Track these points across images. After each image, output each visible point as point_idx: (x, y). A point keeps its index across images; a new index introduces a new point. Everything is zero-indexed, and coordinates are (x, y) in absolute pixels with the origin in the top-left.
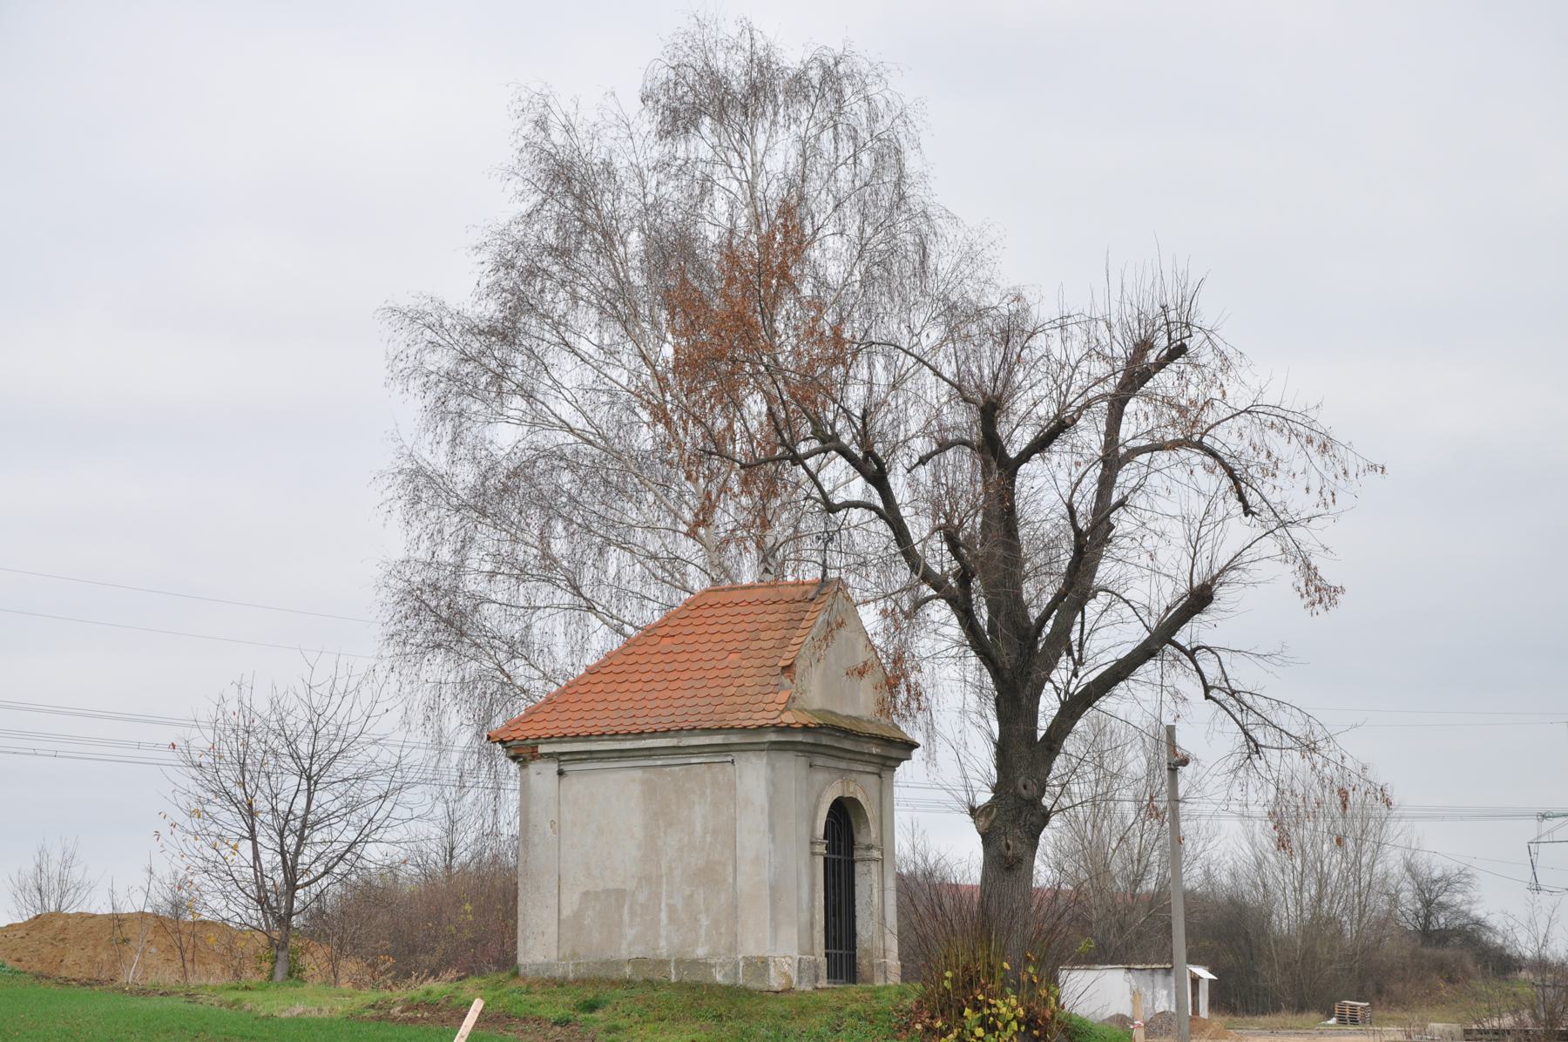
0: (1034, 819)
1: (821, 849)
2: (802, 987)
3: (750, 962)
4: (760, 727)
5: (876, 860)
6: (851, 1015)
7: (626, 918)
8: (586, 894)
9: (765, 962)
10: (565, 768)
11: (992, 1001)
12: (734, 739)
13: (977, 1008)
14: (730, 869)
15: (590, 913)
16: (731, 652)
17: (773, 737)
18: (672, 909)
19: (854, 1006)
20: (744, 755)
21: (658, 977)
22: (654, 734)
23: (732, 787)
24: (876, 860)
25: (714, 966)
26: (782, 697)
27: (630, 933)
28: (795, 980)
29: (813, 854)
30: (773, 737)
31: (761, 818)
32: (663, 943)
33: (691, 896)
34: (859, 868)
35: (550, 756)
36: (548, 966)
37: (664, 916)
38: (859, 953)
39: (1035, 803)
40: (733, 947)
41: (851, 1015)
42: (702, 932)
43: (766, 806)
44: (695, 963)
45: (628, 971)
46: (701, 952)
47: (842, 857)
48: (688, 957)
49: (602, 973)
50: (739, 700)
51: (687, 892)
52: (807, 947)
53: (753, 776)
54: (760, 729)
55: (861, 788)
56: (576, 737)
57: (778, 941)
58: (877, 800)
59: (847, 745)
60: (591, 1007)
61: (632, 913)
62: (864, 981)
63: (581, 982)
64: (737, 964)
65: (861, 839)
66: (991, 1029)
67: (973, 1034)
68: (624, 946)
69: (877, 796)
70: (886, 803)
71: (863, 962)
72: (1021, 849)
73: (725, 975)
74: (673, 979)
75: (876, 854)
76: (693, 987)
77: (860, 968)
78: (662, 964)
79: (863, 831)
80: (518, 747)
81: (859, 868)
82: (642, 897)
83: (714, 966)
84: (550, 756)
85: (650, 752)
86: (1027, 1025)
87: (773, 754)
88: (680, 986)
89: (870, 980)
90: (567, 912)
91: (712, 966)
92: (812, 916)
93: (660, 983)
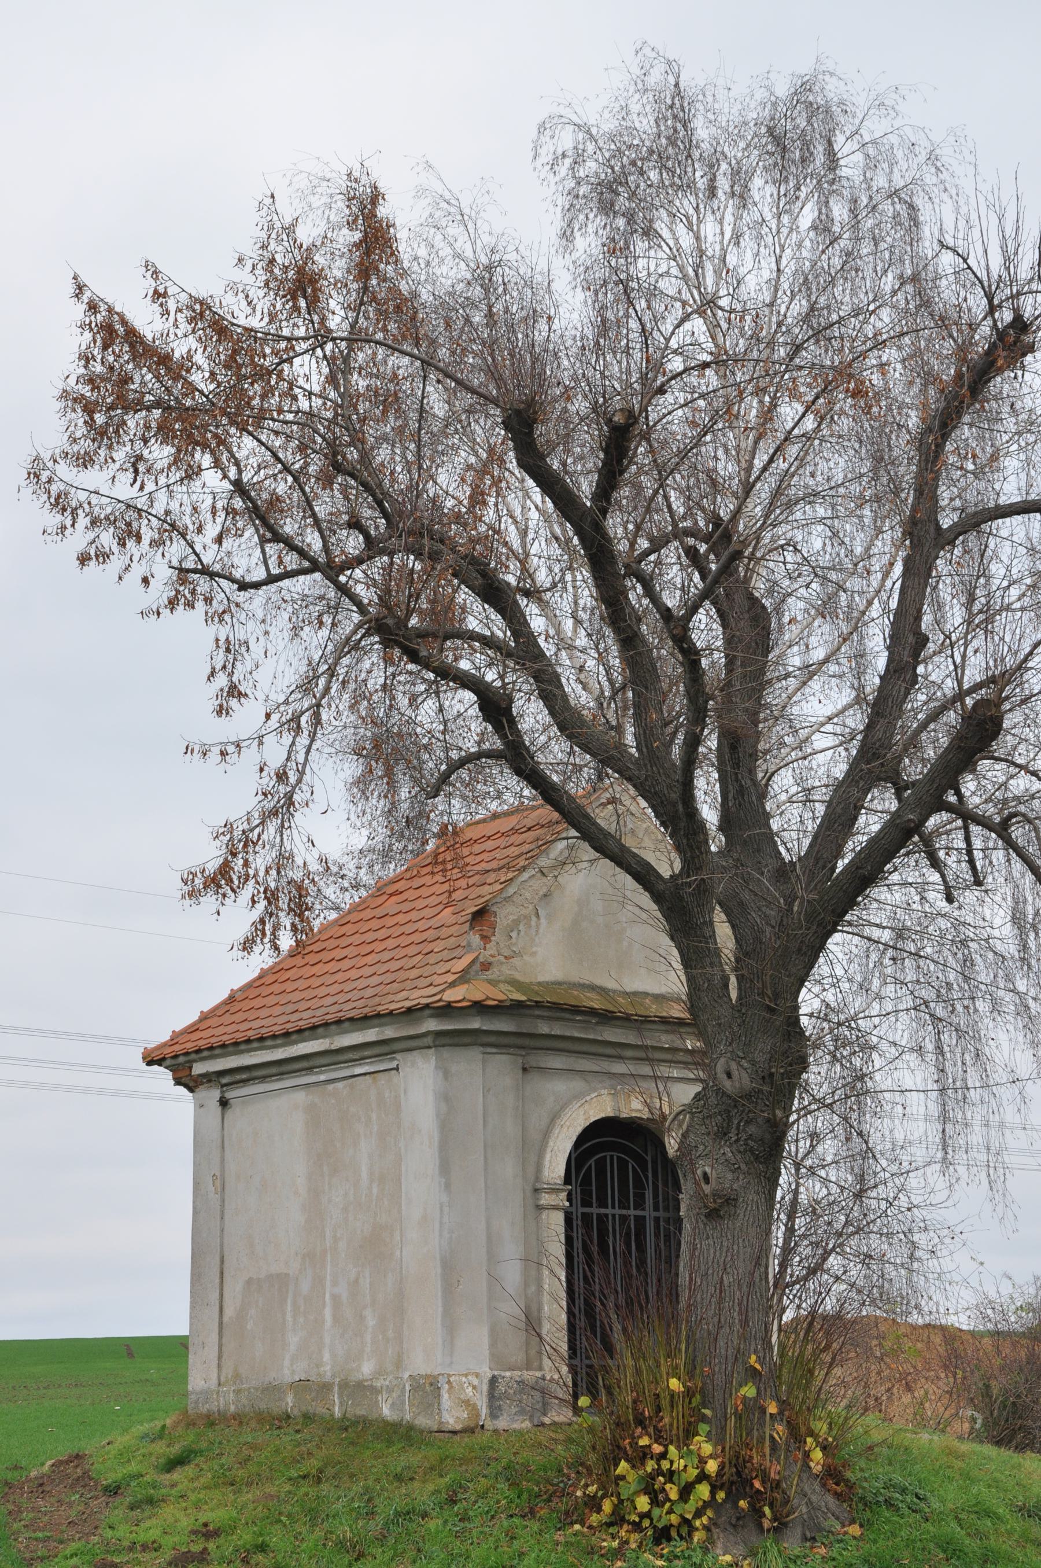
2: (502, 1423)
4: (410, 1010)
8: (249, 1282)
10: (229, 1095)
17: (432, 1025)
18: (335, 1298)
20: (410, 1056)
28: (484, 1411)
30: (432, 1025)
32: (327, 1356)
37: (328, 1313)
42: (368, 1338)
43: (436, 1138)
46: (367, 1369)
53: (419, 1083)
74: (337, 1412)
82: (305, 1286)
85: (307, 1063)
87: (446, 1052)
88: (345, 1425)
91: (376, 1391)
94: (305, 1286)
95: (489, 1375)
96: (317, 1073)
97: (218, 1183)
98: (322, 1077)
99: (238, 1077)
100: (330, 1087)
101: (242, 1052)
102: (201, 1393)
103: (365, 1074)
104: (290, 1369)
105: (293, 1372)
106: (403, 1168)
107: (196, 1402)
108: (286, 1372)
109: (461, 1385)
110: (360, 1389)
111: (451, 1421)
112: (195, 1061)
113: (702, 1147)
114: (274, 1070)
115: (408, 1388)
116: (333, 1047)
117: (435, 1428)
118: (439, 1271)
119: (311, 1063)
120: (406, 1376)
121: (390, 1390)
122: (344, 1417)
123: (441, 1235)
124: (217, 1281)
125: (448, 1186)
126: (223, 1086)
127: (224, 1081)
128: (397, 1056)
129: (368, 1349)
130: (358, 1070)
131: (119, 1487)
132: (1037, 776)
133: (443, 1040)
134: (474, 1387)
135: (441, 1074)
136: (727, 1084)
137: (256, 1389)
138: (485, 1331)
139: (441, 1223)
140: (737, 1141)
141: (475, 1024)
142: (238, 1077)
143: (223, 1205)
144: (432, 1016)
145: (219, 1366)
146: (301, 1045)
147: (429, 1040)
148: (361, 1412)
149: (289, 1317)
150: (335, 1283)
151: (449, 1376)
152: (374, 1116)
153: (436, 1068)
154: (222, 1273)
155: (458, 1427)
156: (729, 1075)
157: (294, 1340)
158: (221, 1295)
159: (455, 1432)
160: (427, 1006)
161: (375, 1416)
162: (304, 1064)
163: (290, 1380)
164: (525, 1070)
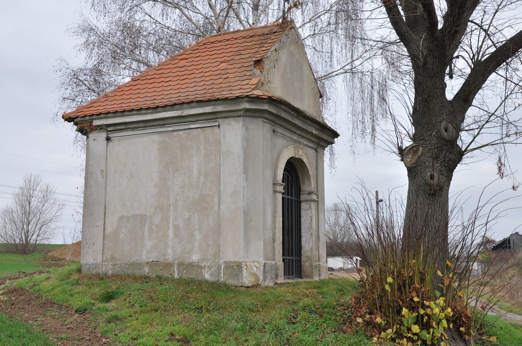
0: (451, 156)
1: (280, 189)
2: (267, 283)
3: (229, 266)
4: (238, 97)
5: (314, 201)
6: (304, 309)
7: (146, 234)
8: (121, 218)
9: (239, 266)
10: (110, 136)
11: (426, 303)
12: (220, 108)
13: (412, 308)
14: (216, 200)
15: (124, 230)
16: (222, 62)
17: (247, 105)
18: (176, 228)
19: (306, 301)
20: (227, 121)
21: (165, 274)
22: (165, 107)
23: (218, 143)
24: (314, 201)
25: (204, 268)
26: (255, 81)
27: (149, 244)
28: (261, 278)
29: (275, 192)
30: (247, 105)
31: (238, 160)
32: (170, 251)
33: (189, 219)
34: (304, 206)
35: (100, 128)
36: (96, 265)
37: (171, 233)
38: (303, 258)
39: (452, 143)
40: (217, 255)
41: (304, 309)
42: (197, 244)
44: (191, 265)
45: (146, 269)
46: (195, 258)
47: (293, 198)
48: (187, 261)
49: (130, 271)
50: (224, 85)
51: (187, 216)
52: (270, 255)
53: (233, 134)
54: (238, 98)
55: (306, 155)
56: (115, 113)
57: (250, 251)
58: (315, 165)
59: (298, 122)
60: (109, 297)
61: (151, 231)
62: (307, 277)
63: (116, 277)
64: (220, 266)
65: (305, 188)
66: (426, 326)
67: (409, 329)
68: (144, 253)
69: (314, 163)
70: (320, 168)
71: (306, 264)
72: (285, 257)
73: (211, 274)
74: (176, 276)
75: (314, 197)
76: (188, 282)
77: (304, 268)
78: (169, 265)
79: (307, 183)
80: (82, 122)
81: (304, 206)
82: (157, 220)
83: (204, 268)
84: (100, 128)
86: (454, 322)
87: (247, 119)
88: (180, 282)
89: (311, 276)
90: (109, 230)
92: (274, 234)
93: (167, 279)
95: (263, 262)
96: (167, 127)
97: (104, 174)
98: (170, 129)
99: (118, 128)
101: (125, 116)
102: (92, 264)
103: (197, 128)
105: (149, 258)
106: (222, 170)
107: (89, 268)
108: (144, 257)
109: (251, 266)
111: (247, 282)
112: (95, 119)
113: (427, 163)
115: (223, 267)
116: (183, 114)
117: (240, 285)
118: (242, 216)
119: (165, 122)
120: (222, 261)
121: (210, 267)
122: (180, 279)
123: (243, 200)
124: (103, 216)
125: (247, 179)
126: (108, 131)
127: (109, 129)
128: (219, 120)
129: (196, 249)
131: (86, 310)
133: (250, 113)
134: (257, 268)
135: (244, 129)
136: (445, 134)
137: (126, 264)
138: (262, 243)
139: (244, 195)
140: (444, 161)
141: (266, 107)
142: (118, 128)
143: (106, 184)
144: (247, 102)
145: (103, 254)
147: (241, 113)
151: (247, 262)
152: (202, 146)
153: (243, 126)
154: (105, 213)
155: (250, 285)
156: (446, 130)
158: (105, 223)
159: (248, 287)
160: (247, 96)
161: (200, 278)
162: (161, 122)
163: (146, 261)
164: (274, 131)
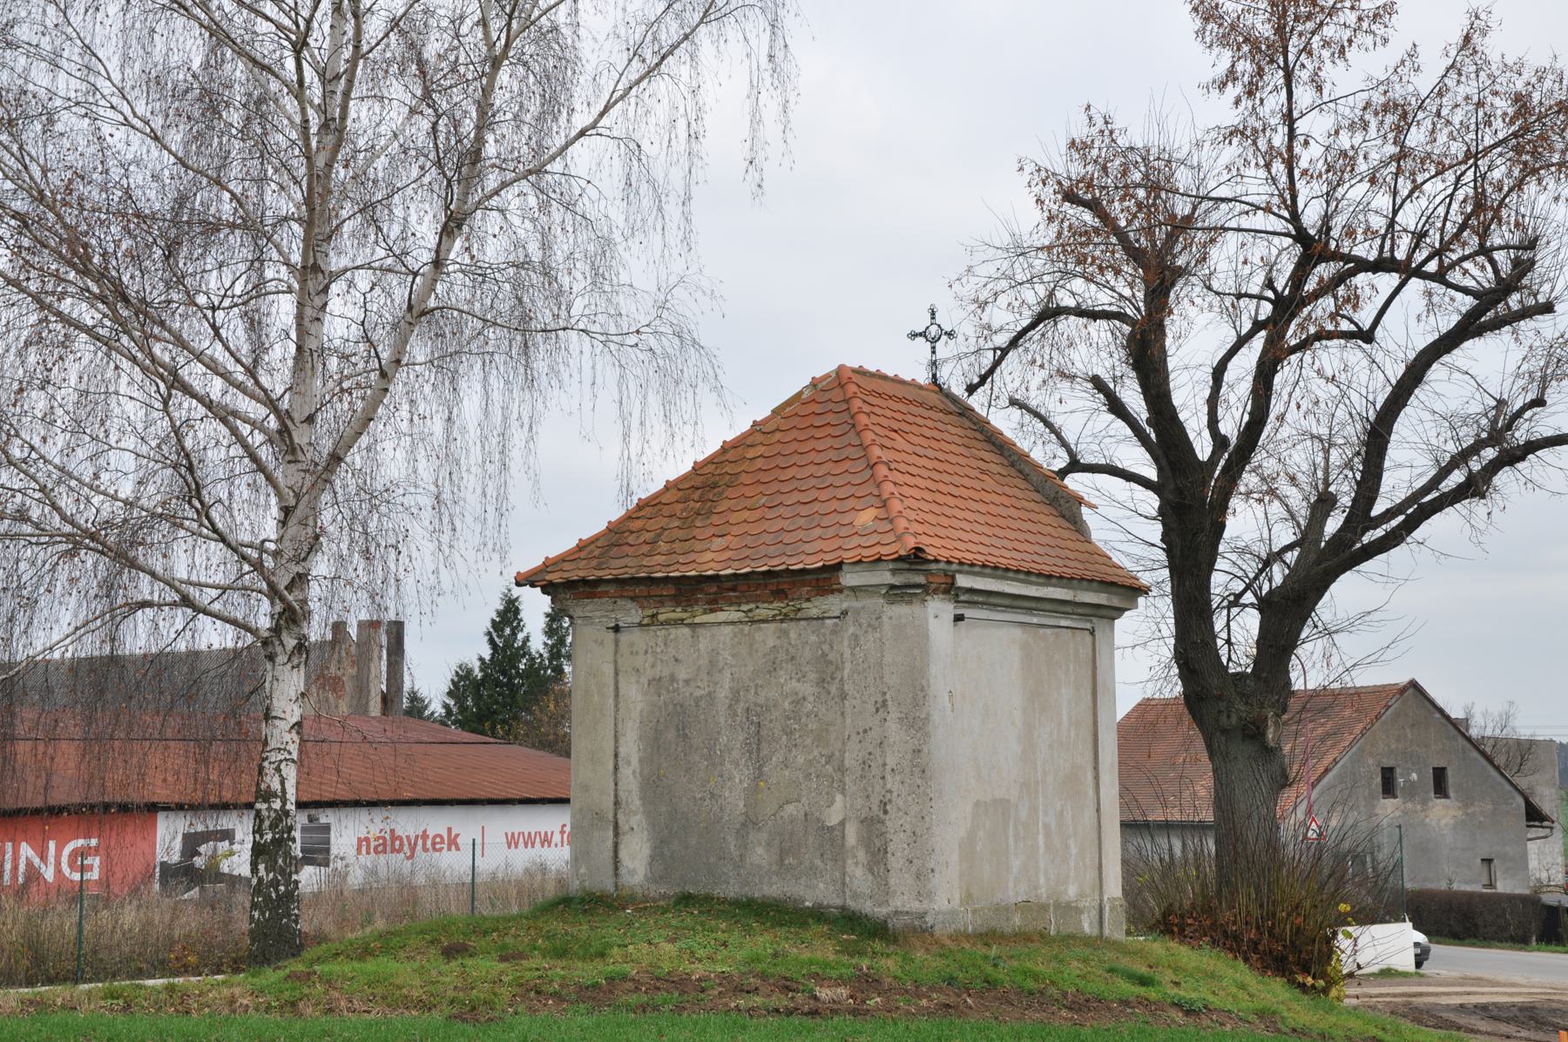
18: (1046, 826)
32: (1042, 880)
37: (1041, 839)
42: (1072, 864)
46: (1072, 891)
82: (1023, 814)
94: (1023, 814)
98: (1035, 620)
100: (1041, 631)
104: (1014, 892)
110: (1069, 910)
114: (1007, 602)
130: (1063, 623)
132: (5, 278)
146: (1051, 589)
148: (1070, 930)
149: (1011, 842)
150: (1046, 814)
157: (1016, 863)
